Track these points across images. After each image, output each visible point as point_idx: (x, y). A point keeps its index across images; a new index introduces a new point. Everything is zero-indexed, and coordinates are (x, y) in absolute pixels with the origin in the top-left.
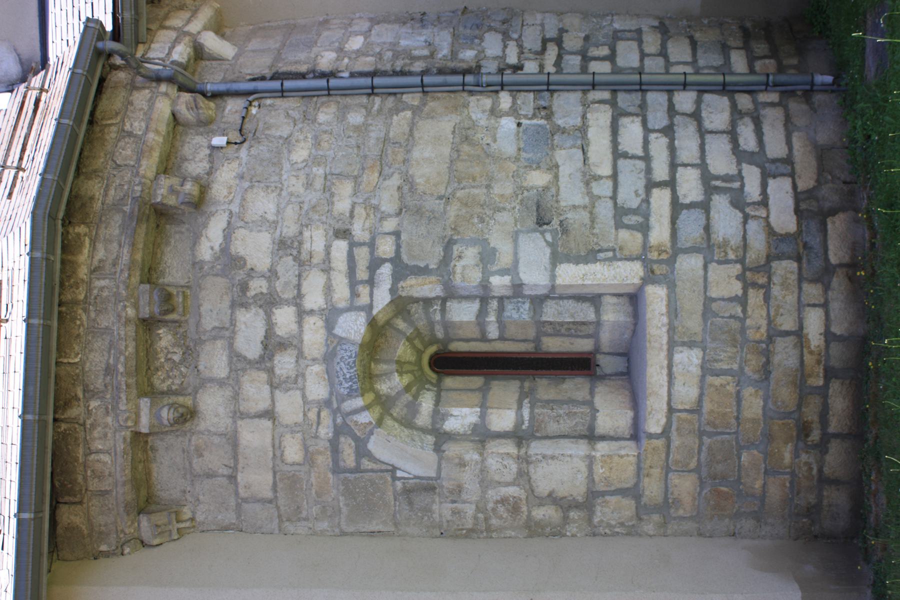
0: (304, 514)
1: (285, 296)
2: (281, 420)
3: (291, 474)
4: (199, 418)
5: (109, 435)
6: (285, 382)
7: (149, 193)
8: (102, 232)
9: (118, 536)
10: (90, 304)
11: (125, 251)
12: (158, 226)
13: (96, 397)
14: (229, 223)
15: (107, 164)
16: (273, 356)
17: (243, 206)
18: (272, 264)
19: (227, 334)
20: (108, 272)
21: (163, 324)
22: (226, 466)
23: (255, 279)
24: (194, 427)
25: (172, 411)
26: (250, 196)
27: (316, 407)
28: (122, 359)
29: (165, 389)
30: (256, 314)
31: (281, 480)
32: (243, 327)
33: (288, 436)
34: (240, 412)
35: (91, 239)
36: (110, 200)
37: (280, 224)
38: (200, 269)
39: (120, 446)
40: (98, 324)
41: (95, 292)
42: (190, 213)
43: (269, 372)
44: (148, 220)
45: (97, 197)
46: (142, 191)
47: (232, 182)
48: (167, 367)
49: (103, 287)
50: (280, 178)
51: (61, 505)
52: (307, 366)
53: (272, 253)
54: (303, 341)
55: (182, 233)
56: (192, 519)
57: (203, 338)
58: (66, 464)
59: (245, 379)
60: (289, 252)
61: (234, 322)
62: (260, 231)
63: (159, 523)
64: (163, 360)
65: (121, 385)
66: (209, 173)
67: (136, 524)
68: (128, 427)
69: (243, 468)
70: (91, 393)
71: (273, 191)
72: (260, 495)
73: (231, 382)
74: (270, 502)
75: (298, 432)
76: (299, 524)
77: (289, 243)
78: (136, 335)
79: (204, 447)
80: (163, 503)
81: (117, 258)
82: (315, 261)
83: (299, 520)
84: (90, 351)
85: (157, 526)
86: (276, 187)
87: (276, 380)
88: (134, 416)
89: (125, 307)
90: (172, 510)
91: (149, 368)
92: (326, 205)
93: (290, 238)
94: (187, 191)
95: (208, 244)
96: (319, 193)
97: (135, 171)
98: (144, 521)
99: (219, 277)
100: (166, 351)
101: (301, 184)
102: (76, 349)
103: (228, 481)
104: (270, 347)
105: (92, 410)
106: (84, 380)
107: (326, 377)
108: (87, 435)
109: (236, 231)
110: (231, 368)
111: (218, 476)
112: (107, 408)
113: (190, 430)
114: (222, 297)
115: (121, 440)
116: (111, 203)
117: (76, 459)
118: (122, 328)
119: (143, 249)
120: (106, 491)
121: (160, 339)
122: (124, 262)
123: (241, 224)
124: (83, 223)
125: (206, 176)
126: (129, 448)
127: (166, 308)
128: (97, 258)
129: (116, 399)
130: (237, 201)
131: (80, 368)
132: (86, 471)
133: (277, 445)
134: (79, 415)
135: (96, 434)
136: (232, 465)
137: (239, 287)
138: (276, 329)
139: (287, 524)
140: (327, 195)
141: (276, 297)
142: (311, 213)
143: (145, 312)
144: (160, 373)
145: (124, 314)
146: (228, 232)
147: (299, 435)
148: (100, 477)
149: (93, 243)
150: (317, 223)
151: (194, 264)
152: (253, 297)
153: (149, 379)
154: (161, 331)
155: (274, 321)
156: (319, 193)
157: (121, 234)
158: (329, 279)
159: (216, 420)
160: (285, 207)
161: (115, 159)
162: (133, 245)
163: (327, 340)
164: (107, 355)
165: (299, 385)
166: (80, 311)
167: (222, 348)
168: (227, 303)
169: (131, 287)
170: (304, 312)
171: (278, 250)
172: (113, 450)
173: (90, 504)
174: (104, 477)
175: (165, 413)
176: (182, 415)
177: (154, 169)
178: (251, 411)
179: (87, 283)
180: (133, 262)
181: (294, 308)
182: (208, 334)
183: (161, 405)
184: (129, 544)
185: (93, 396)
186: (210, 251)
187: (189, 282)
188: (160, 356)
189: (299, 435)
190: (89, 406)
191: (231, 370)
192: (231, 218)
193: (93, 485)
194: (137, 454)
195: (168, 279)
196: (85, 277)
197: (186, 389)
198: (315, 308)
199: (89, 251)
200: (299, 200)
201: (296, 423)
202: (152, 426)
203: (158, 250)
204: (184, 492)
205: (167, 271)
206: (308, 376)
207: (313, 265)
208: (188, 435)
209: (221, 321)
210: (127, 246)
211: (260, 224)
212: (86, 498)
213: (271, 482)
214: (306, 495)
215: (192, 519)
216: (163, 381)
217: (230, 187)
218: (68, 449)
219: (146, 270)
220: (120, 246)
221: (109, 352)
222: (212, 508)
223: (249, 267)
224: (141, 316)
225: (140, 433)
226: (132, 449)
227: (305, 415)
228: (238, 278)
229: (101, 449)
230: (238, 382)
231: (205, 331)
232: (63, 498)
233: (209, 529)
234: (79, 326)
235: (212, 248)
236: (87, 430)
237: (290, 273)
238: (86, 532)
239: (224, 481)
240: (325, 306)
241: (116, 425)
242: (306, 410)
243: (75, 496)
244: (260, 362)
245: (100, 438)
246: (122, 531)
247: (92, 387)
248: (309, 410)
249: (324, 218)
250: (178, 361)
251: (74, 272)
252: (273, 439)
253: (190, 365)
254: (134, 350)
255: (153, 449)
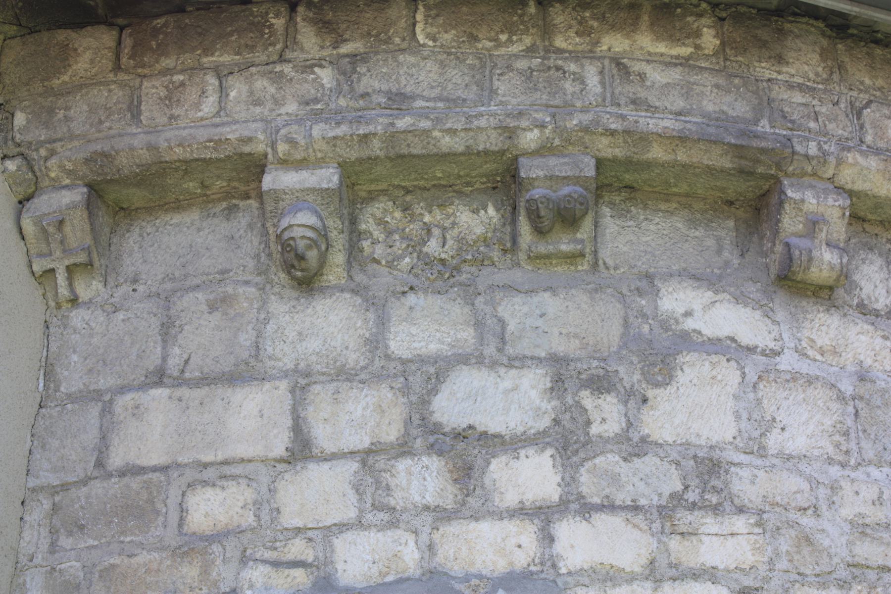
0: (65, 542)
1: (584, 477)
2: (287, 476)
3: (160, 506)
4: (297, 299)
5: (258, 110)
6: (378, 482)
7: (804, 174)
8: (707, 80)
9: (41, 144)
10: (544, 58)
11: (667, 123)
12: (731, 203)
13: (341, 78)
14: (751, 350)
15: (861, 91)
16: (440, 453)
17: (794, 379)
18: (661, 445)
19: (490, 350)
20: (617, 91)
21: (508, 215)
22: (187, 362)
23: (621, 407)
24: (276, 289)
25: (310, 234)
26: (819, 393)
27: (316, 558)
28: (425, 124)
29: (363, 227)
30: (538, 413)
31: (147, 485)
32: (507, 384)
33: (249, 495)
34: (308, 385)
35: (688, 59)
36: (780, 93)
37: (759, 462)
38: (638, 289)
39: (233, 131)
40: (501, 74)
41: (573, 67)
42: (767, 266)
43: (401, 445)
44: (741, 171)
45: (785, 69)
46: (807, 157)
47: (848, 357)
48: (414, 228)
49: (583, 82)
50: (870, 463)
51: (115, 33)
52: (416, 532)
53: (687, 444)
54: (477, 520)
55: (719, 252)
56: (74, 301)
57: (480, 300)
58: (200, 34)
59: (385, 393)
60: (694, 482)
61: (516, 363)
62: (738, 417)
63: (67, 229)
64: (427, 219)
65: (367, 124)
66: (864, 310)
67: (67, 181)
68: (273, 145)
69: (180, 400)
70: (349, 68)
71: (837, 446)
72: (116, 441)
73: (378, 363)
74: (100, 464)
75: (258, 517)
76: (44, 532)
77: (715, 482)
78: (479, 153)
79: (232, 312)
80: (115, 240)
81: (652, 109)
82: (674, 543)
83: (53, 532)
84: (442, 62)
85: (61, 222)
86: (847, 452)
87: (381, 462)
88: (298, 157)
89: (542, 126)
90: (95, 255)
91: (408, 192)
92: (818, 570)
93: (727, 484)
94: (816, 253)
95: (697, 306)
96: (844, 553)
97: (851, 144)
98: (75, 196)
99: (622, 330)
100: (447, 224)
101: (863, 510)
102: (446, 36)
103: (151, 368)
104: (461, 446)
105: (313, 73)
106: (377, 53)
107: (390, 578)
108: (259, 68)
109: (733, 363)
110: (410, 361)
111: (164, 348)
112: (316, 101)
113: (270, 282)
114: (576, 336)
115: (247, 133)
116: (773, 95)
117: (208, 52)
118: (493, 122)
119: (674, 164)
120: (139, 113)
121: (475, 211)
122: (642, 120)
123: (752, 377)
124: (723, 44)
125: (856, 301)
126: (229, 151)
127: (542, 213)
128: (648, 69)
129: (337, 117)
130: (804, 367)
131: (405, 45)
132: (182, 71)
133: (228, 470)
134: (302, 49)
135: (261, 83)
136: (187, 375)
137: (601, 372)
138: (504, 459)
139: (47, 505)
140: (843, 573)
141: (582, 455)
142: (793, 533)
143: (530, 169)
144: (398, 214)
145: (524, 123)
146: (729, 347)
147: (250, 519)
148: (170, 98)
149: (683, 62)
150: (769, 549)
151: (649, 277)
152: (578, 404)
153: (384, 192)
154: (491, 211)
155: (522, 453)
156: (844, 553)
157: (705, 115)
158: (631, 578)
159: (292, 335)
160: (800, 473)
161: (874, 106)
162: (682, 139)
163: (480, 577)
164: (433, 95)
165: (369, 516)
166: (528, 41)
167: (458, 340)
168: (561, 347)
169: (587, 138)
170: (548, 522)
171: (695, 457)
172: (225, 119)
173: (113, 87)
174: (169, 107)
175: (306, 218)
176: (301, 258)
177: (859, 186)
178: (311, 409)
179: (591, 51)
180: (645, 139)
181: (556, 498)
182: (488, 309)
183: (324, 214)
184: (24, 169)
185: (344, 73)
186: (682, 310)
187: (607, 268)
188: (437, 212)
189: (250, 519)
190: (321, 66)
191: (404, 362)
192: (763, 353)
193: (154, 87)
194: (219, 177)
195: (610, 224)
196: (605, 48)
197: (363, 270)
198: (559, 547)
199: (662, 55)
200: (824, 507)
201: (278, 511)
202: (277, 195)
203: (675, 205)
204: (135, 281)
205: (631, 223)
206: (392, 534)
207: (665, 539)
208: (258, 279)
209: (520, 338)
210: (678, 126)
211: (755, 416)
212: (126, 77)
213: (145, 462)
214: (109, 543)
215: (74, 301)
216: (380, 222)
217: (835, 352)
218: (231, 34)
219: (628, 177)
220: (680, 113)
221: (440, 99)
222: (95, 340)
223: (650, 393)
224: (522, 161)
225: (263, 172)
226: (228, 157)
227: (298, 531)
228: (622, 370)
229: (227, 95)
230: (378, 378)
231: (493, 304)
232: (131, 35)
233: (52, 338)
234: (496, 40)
235: (688, 314)
236: (270, 67)
237: (641, 486)
238: (56, 82)
239: (153, 361)
240: (564, 571)
241: (280, 121)
242: (310, 534)
243: (132, 57)
244: (425, 426)
245: (251, 93)
246: (52, 153)
247: (362, 69)
248: (310, 540)
249: (783, 564)
250: (425, 249)
251: (613, 27)
252: (243, 460)
253: (416, 276)
254: (445, 150)
255: (232, 210)
